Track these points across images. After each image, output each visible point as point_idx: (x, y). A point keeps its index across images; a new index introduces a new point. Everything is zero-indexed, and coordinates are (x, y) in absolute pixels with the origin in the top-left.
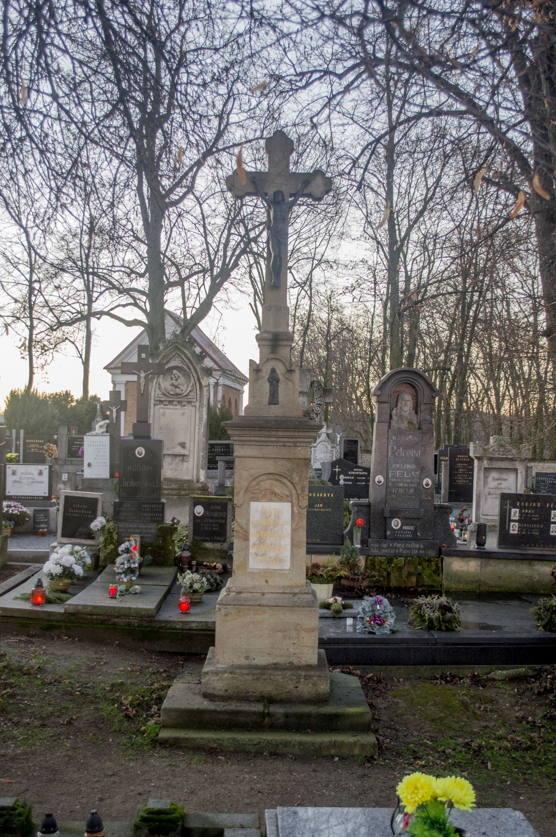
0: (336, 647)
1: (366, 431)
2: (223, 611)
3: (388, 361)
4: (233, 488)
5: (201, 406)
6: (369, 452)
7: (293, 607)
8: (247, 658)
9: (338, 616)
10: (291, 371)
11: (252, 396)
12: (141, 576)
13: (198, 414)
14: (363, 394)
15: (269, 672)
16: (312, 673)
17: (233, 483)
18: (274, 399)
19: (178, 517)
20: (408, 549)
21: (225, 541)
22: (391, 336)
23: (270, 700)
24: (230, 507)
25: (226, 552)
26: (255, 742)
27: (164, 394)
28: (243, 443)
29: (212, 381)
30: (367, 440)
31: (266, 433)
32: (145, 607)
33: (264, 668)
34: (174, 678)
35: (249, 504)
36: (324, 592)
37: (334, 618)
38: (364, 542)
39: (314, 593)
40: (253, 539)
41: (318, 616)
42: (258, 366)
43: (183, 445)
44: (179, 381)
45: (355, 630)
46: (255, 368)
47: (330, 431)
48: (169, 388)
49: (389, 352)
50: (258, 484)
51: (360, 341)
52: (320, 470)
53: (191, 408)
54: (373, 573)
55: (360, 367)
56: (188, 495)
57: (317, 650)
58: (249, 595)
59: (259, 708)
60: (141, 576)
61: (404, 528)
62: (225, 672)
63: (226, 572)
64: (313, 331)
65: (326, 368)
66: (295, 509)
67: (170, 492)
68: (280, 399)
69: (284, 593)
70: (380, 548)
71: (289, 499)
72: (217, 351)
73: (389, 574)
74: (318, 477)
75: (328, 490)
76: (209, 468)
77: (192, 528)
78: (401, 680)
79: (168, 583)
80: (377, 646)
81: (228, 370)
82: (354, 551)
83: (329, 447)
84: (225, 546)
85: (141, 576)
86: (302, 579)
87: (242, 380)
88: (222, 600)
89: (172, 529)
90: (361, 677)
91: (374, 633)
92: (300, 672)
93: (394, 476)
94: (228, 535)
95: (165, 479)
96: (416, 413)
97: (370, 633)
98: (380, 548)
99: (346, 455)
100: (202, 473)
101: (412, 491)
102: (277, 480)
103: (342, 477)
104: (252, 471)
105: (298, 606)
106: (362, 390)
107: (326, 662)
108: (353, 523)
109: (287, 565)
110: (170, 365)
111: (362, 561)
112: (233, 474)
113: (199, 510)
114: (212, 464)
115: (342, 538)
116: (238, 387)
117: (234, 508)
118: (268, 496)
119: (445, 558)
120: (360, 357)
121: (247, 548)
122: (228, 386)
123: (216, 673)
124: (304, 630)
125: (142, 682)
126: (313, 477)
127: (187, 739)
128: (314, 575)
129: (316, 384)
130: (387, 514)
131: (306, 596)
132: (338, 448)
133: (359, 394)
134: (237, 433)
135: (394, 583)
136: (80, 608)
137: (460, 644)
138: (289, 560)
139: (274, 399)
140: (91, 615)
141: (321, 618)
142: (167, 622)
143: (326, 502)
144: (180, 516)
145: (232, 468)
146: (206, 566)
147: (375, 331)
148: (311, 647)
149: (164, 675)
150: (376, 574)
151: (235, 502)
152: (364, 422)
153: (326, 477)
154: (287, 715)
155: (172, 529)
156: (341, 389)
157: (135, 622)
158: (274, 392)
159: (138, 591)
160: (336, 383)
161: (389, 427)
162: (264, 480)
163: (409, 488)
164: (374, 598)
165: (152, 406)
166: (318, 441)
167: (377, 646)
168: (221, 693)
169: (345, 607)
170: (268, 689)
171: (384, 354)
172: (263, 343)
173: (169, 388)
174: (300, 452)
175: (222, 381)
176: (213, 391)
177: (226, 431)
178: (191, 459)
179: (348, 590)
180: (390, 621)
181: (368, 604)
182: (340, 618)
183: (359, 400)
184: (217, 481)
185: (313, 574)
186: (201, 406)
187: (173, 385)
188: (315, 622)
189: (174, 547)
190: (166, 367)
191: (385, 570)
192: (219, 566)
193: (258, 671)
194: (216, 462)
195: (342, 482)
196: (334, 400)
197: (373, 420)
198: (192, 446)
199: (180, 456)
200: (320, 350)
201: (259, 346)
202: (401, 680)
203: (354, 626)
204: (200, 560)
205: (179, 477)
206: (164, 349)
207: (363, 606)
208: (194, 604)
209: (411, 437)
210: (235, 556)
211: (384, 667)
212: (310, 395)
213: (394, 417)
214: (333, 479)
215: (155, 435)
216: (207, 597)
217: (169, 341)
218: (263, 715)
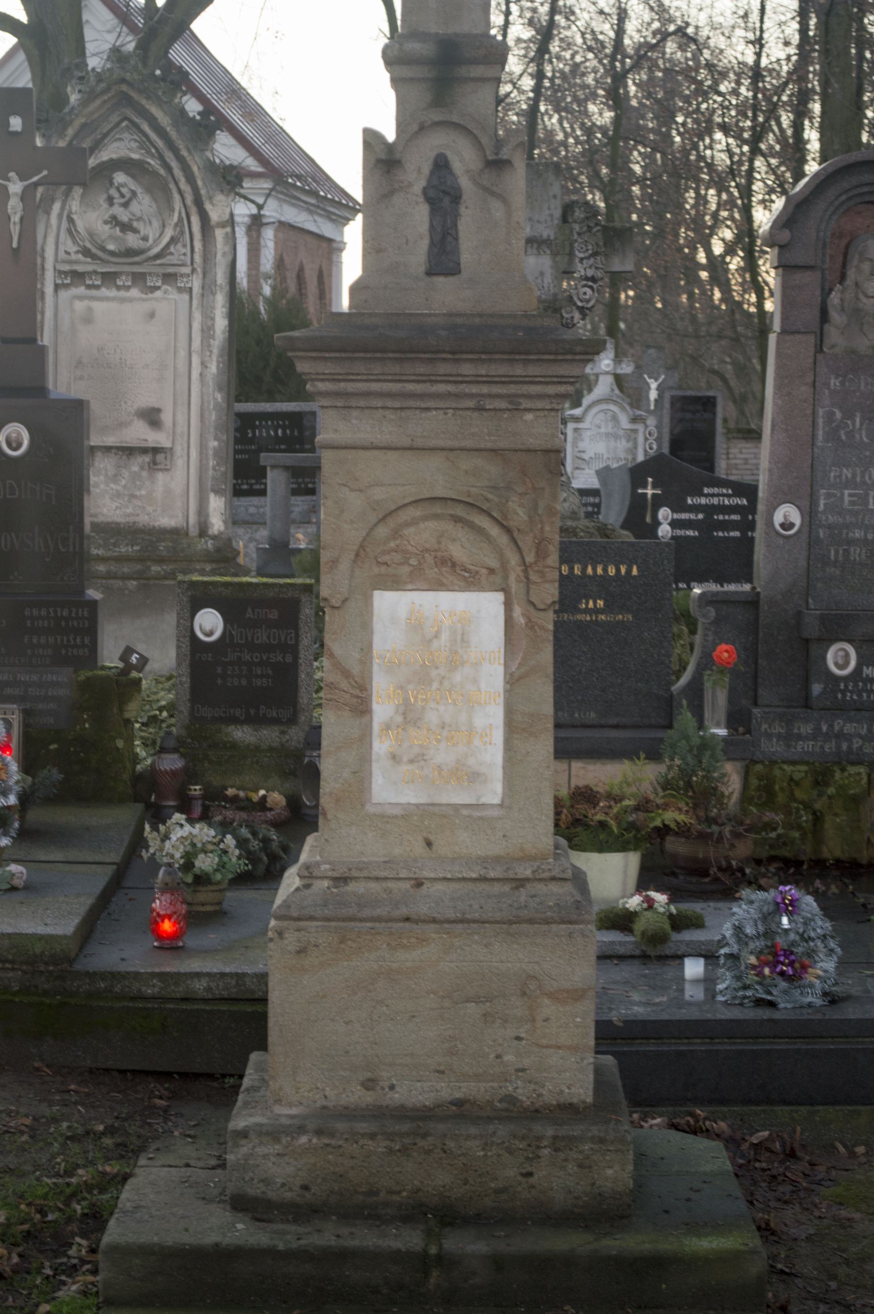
0: (651, 1047)
1: (741, 370)
2: (291, 939)
3: (812, 137)
4: (315, 554)
5: (208, 288)
6: (754, 435)
7: (515, 923)
8: (369, 1084)
9: (656, 951)
10: (497, 165)
11: (373, 248)
12: (26, 835)
13: (197, 316)
14: (730, 250)
15: (441, 1127)
16: (576, 1130)
17: (318, 536)
18: (443, 259)
19: (141, 647)
21: (293, 720)
22: (826, 52)
23: (446, 1216)
24: (307, 611)
25: (297, 755)
27: (86, 252)
28: (346, 402)
29: (243, 210)
30: (744, 398)
31: (422, 369)
32: (41, 930)
33: (422, 1116)
34: (142, 1149)
35: (368, 601)
36: (611, 874)
37: (644, 958)
38: (737, 719)
39: (579, 880)
40: (382, 710)
41: (592, 952)
42: (390, 148)
43: (152, 417)
44: (135, 207)
45: (711, 993)
46: (381, 158)
47: (627, 368)
48: (104, 231)
49: (816, 107)
50: (396, 533)
51: (724, 75)
52: (595, 493)
53: (174, 295)
54: (769, 816)
55: (722, 159)
56: (172, 575)
57: (590, 1058)
58: (374, 886)
59: (408, 1239)
60: (26, 835)
62: (301, 1129)
63: (301, 818)
64: (567, 44)
65: (613, 166)
66: (517, 612)
67: (113, 567)
68: (466, 257)
69: (483, 879)
70: (789, 738)
71: (498, 579)
72: (254, 112)
73: (818, 818)
74: (588, 515)
75: (620, 555)
76: (238, 493)
77: (186, 679)
78: (861, 1150)
79: (115, 856)
80: (781, 1045)
81: (295, 177)
82: (706, 745)
83: (624, 421)
84: (295, 735)
85: (28, 835)
86: (540, 833)
87: (339, 207)
88: (286, 904)
89: (124, 684)
90: (732, 1143)
91: (772, 1004)
92: (538, 1128)
94: (303, 699)
95: (95, 526)
97: (759, 1002)
98: (789, 738)
99: (676, 445)
100: (216, 505)
102: (457, 519)
103: (664, 513)
104: (378, 493)
105: (531, 921)
106: (728, 235)
107: (621, 1095)
108: (704, 661)
109: (493, 792)
110: (105, 155)
111: (732, 780)
112: (314, 510)
113: (210, 622)
114: (245, 477)
115: (667, 709)
116: (326, 229)
117: (319, 613)
120: (725, 128)
121: (365, 738)
122: (292, 227)
123: (273, 1133)
124: (550, 995)
125: (37, 1167)
126: (574, 516)
128: (579, 823)
129: (579, 214)
130: (812, 629)
131: (554, 887)
132: (652, 422)
133: (718, 248)
134: (329, 368)
135: (833, 848)
138: (498, 773)
139: (443, 259)
141: (603, 957)
143: (614, 592)
144: (149, 644)
145: (312, 492)
146: (235, 799)
147: (772, 36)
148: (573, 1049)
149: (108, 1141)
150: (779, 818)
151: (325, 591)
152: (736, 339)
153: (613, 514)
154: (498, 1263)
155: (124, 684)
156: (659, 234)
158: (445, 234)
159: (16, 882)
160: (641, 213)
161: (819, 349)
162: (414, 522)
164: (770, 895)
165: (49, 289)
166: (586, 401)
167: (781, 1045)
168: (288, 1195)
169: (679, 923)
170: (439, 1180)
171: (801, 113)
172: (406, 72)
173: (104, 231)
174: (532, 429)
175: (273, 211)
176: (245, 238)
177: (291, 366)
178: (180, 462)
179: (688, 870)
180: (826, 964)
181: (753, 912)
182: (663, 958)
183: (716, 265)
184: (263, 533)
185: (576, 822)
186: (208, 288)
187: (114, 221)
188: (582, 971)
189: (130, 740)
190: (92, 162)
191: (807, 806)
192: (277, 799)
193: (406, 1127)
194: (262, 473)
195: (664, 530)
196: (638, 266)
197: (763, 331)
198: (181, 418)
199: (144, 451)
200: (592, 108)
201: (395, 82)
202: (861, 1150)
203: (708, 981)
204: (216, 781)
205: (143, 520)
206: (84, 103)
207: (734, 919)
208: (196, 919)
210: (327, 766)
211: (804, 1109)
212: (560, 249)
213: (835, 316)
214: (639, 519)
215: (62, 383)
216: (235, 898)
217: (99, 77)
218: (423, 1262)
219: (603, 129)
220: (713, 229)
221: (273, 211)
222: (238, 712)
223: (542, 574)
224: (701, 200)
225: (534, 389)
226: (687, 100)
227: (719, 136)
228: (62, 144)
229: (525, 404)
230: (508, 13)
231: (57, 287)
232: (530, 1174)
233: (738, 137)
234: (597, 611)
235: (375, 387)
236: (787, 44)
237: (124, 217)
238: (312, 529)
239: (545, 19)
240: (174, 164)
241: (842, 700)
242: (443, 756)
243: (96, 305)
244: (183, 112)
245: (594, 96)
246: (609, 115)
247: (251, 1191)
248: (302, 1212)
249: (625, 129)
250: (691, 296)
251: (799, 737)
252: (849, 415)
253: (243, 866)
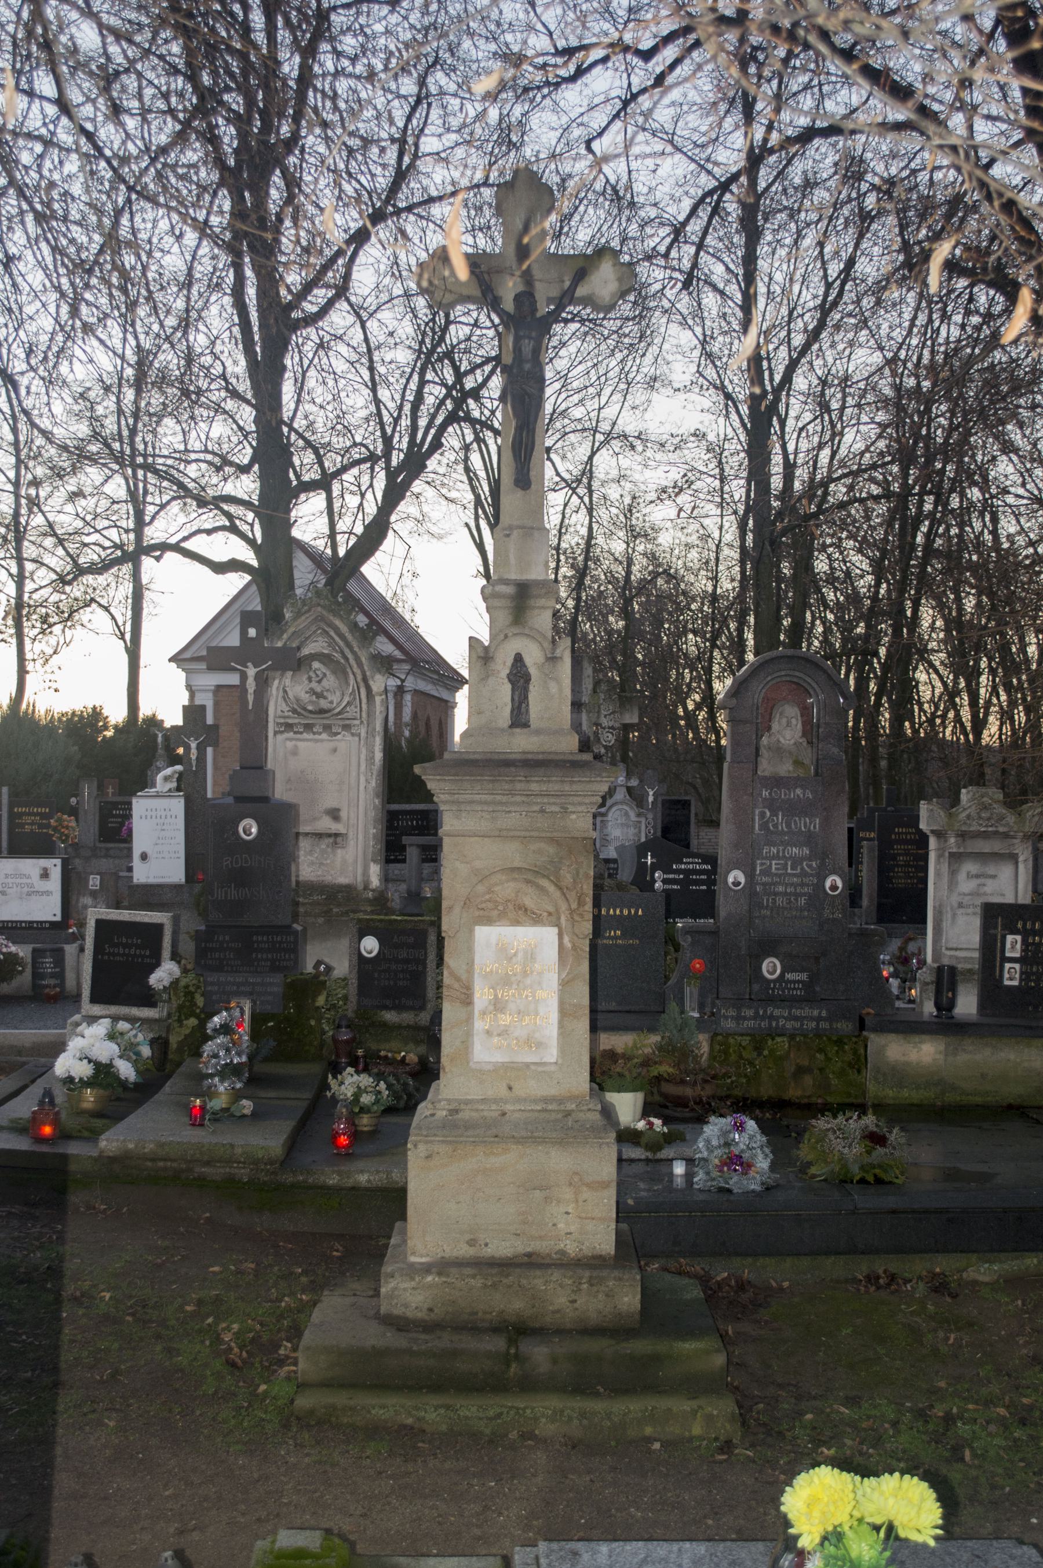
3: (749, 637)
6: (715, 824)
8: (472, 1243)
11: (474, 711)
13: (364, 750)
14: (698, 706)
18: (519, 719)
21: (422, 1008)
22: (757, 586)
27: (294, 711)
35: (471, 931)
43: (334, 814)
44: (325, 683)
47: (634, 783)
49: (751, 619)
50: (490, 891)
51: (693, 599)
52: (615, 861)
53: (349, 738)
61: (789, 976)
63: (427, 1072)
64: (595, 579)
65: (624, 655)
66: (566, 940)
70: (738, 1018)
71: (553, 919)
72: (400, 621)
76: (388, 861)
84: (424, 1018)
86: (580, 1081)
89: (316, 983)
93: (766, 872)
99: (666, 831)
101: (802, 901)
102: (528, 882)
104: (478, 864)
109: (551, 1054)
113: (370, 945)
114: (392, 851)
116: (444, 694)
119: (872, 1036)
120: (695, 632)
121: (469, 1019)
124: (588, 1185)
128: (604, 1072)
132: (650, 816)
133: (691, 706)
139: (519, 719)
140: (153, 1160)
156: (654, 697)
163: (797, 895)
164: (729, 1120)
165: (271, 734)
168: (420, 1315)
169: (669, 1139)
171: (742, 623)
173: (305, 697)
175: (410, 683)
183: (690, 717)
184: (403, 887)
186: (370, 733)
193: (495, 1271)
194: (403, 848)
196: (641, 718)
199: (329, 835)
200: (611, 619)
204: (374, 1046)
205: (328, 879)
206: (295, 619)
209: (799, 791)
210: (446, 1038)
213: (763, 751)
219: (618, 632)
220: (688, 696)
221: (410, 683)
222: (388, 1002)
223: (581, 916)
224: (680, 676)
225: (576, 799)
226: (670, 614)
227: (691, 636)
228: (280, 644)
229: (571, 808)
230: (558, 561)
231: (276, 733)
232: (574, 1301)
233: (703, 637)
234: (616, 938)
236: (733, 580)
237: (318, 689)
238: (434, 884)
239: (581, 564)
240: (350, 656)
243: (300, 744)
244: (356, 624)
245: (612, 612)
246: (621, 623)
248: (429, 1327)
249: (632, 631)
250: (674, 736)
251: (745, 1018)
253: (391, 1101)
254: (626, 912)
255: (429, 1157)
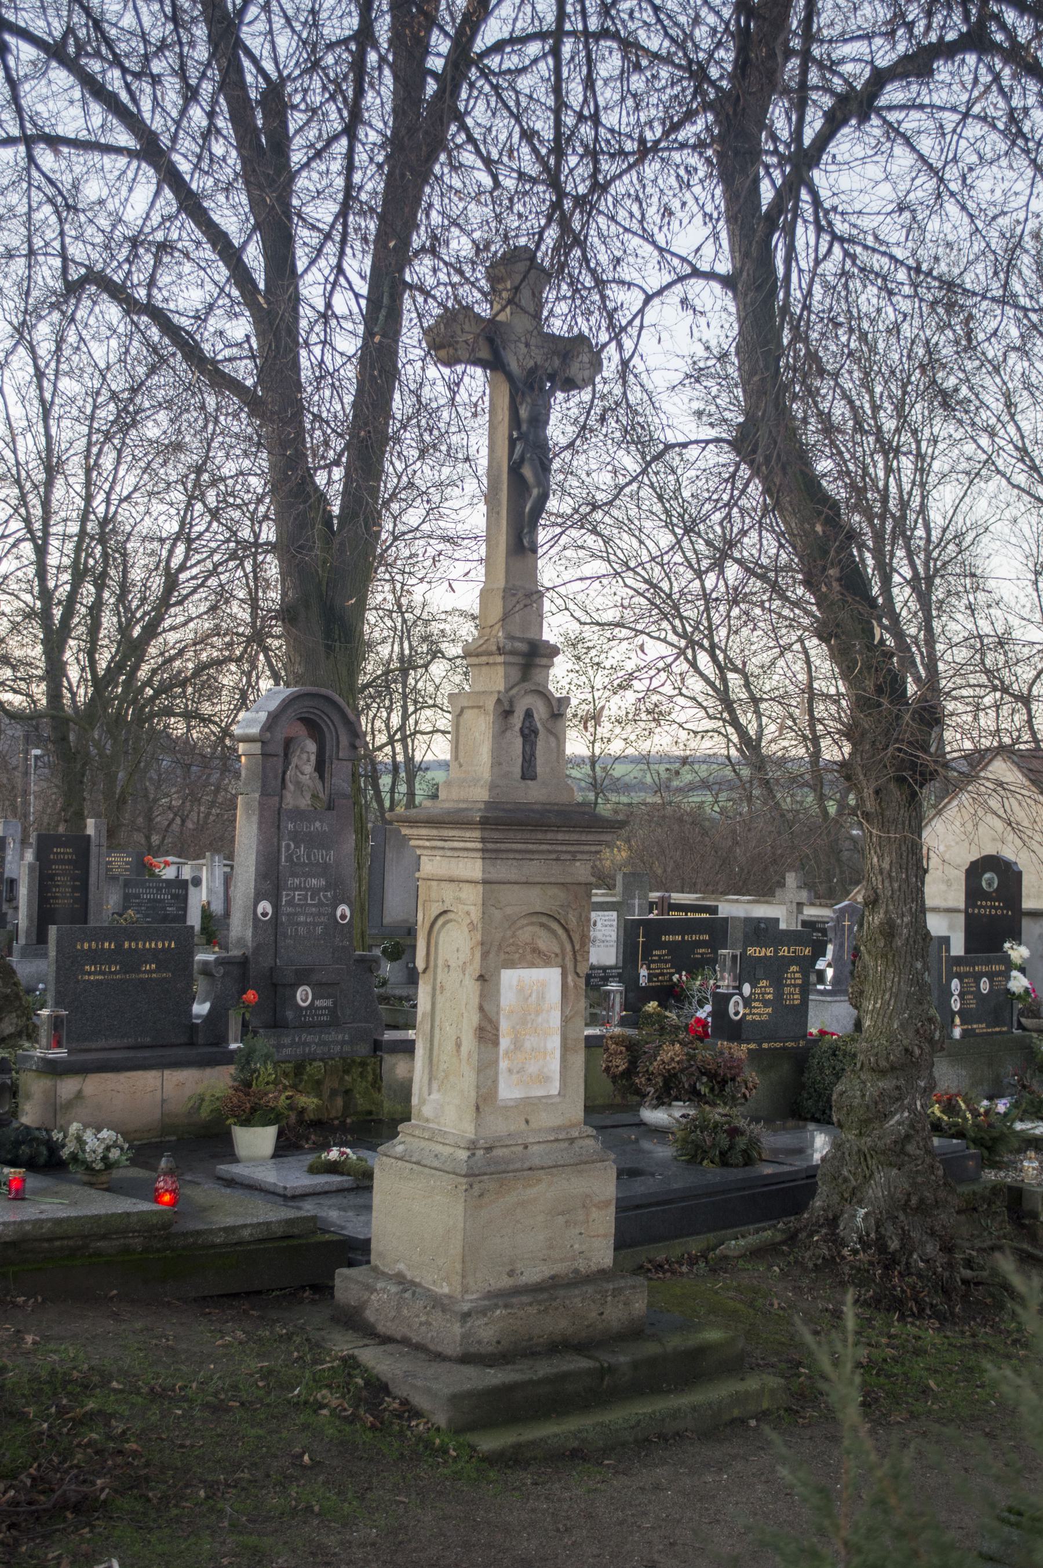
8: (511, 1273)
20: (325, 1043)
26: (633, 1422)
50: (514, 936)
61: (317, 1003)
68: (539, 770)
93: (290, 903)
96: (322, 777)
101: (319, 930)
104: (509, 910)
109: (554, 1088)
118: (529, 957)
119: (386, 1056)
124: (597, 1206)
127: (533, 1443)
136: (28, 1227)
137: (650, 1205)
140: (50, 1240)
142: (198, 1233)
148: (605, 1236)
157: (137, 1242)
163: (315, 924)
168: (490, 1349)
193: (545, 1296)
209: (318, 824)
225: (586, 848)
234: (151, 972)
235: (514, 846)
241: (307, 1022)
242: (532, 1068)
247: (472, 1350)
252: (297, 847)
254: (86, 946)
255: (481, 1195)
